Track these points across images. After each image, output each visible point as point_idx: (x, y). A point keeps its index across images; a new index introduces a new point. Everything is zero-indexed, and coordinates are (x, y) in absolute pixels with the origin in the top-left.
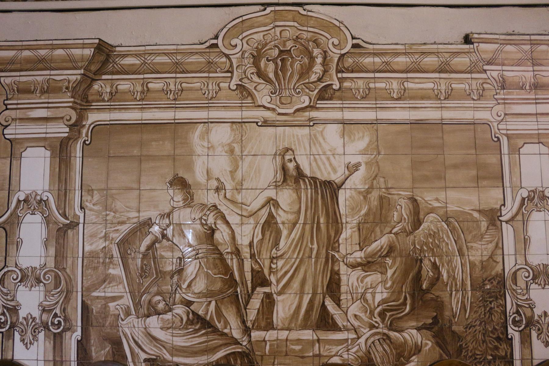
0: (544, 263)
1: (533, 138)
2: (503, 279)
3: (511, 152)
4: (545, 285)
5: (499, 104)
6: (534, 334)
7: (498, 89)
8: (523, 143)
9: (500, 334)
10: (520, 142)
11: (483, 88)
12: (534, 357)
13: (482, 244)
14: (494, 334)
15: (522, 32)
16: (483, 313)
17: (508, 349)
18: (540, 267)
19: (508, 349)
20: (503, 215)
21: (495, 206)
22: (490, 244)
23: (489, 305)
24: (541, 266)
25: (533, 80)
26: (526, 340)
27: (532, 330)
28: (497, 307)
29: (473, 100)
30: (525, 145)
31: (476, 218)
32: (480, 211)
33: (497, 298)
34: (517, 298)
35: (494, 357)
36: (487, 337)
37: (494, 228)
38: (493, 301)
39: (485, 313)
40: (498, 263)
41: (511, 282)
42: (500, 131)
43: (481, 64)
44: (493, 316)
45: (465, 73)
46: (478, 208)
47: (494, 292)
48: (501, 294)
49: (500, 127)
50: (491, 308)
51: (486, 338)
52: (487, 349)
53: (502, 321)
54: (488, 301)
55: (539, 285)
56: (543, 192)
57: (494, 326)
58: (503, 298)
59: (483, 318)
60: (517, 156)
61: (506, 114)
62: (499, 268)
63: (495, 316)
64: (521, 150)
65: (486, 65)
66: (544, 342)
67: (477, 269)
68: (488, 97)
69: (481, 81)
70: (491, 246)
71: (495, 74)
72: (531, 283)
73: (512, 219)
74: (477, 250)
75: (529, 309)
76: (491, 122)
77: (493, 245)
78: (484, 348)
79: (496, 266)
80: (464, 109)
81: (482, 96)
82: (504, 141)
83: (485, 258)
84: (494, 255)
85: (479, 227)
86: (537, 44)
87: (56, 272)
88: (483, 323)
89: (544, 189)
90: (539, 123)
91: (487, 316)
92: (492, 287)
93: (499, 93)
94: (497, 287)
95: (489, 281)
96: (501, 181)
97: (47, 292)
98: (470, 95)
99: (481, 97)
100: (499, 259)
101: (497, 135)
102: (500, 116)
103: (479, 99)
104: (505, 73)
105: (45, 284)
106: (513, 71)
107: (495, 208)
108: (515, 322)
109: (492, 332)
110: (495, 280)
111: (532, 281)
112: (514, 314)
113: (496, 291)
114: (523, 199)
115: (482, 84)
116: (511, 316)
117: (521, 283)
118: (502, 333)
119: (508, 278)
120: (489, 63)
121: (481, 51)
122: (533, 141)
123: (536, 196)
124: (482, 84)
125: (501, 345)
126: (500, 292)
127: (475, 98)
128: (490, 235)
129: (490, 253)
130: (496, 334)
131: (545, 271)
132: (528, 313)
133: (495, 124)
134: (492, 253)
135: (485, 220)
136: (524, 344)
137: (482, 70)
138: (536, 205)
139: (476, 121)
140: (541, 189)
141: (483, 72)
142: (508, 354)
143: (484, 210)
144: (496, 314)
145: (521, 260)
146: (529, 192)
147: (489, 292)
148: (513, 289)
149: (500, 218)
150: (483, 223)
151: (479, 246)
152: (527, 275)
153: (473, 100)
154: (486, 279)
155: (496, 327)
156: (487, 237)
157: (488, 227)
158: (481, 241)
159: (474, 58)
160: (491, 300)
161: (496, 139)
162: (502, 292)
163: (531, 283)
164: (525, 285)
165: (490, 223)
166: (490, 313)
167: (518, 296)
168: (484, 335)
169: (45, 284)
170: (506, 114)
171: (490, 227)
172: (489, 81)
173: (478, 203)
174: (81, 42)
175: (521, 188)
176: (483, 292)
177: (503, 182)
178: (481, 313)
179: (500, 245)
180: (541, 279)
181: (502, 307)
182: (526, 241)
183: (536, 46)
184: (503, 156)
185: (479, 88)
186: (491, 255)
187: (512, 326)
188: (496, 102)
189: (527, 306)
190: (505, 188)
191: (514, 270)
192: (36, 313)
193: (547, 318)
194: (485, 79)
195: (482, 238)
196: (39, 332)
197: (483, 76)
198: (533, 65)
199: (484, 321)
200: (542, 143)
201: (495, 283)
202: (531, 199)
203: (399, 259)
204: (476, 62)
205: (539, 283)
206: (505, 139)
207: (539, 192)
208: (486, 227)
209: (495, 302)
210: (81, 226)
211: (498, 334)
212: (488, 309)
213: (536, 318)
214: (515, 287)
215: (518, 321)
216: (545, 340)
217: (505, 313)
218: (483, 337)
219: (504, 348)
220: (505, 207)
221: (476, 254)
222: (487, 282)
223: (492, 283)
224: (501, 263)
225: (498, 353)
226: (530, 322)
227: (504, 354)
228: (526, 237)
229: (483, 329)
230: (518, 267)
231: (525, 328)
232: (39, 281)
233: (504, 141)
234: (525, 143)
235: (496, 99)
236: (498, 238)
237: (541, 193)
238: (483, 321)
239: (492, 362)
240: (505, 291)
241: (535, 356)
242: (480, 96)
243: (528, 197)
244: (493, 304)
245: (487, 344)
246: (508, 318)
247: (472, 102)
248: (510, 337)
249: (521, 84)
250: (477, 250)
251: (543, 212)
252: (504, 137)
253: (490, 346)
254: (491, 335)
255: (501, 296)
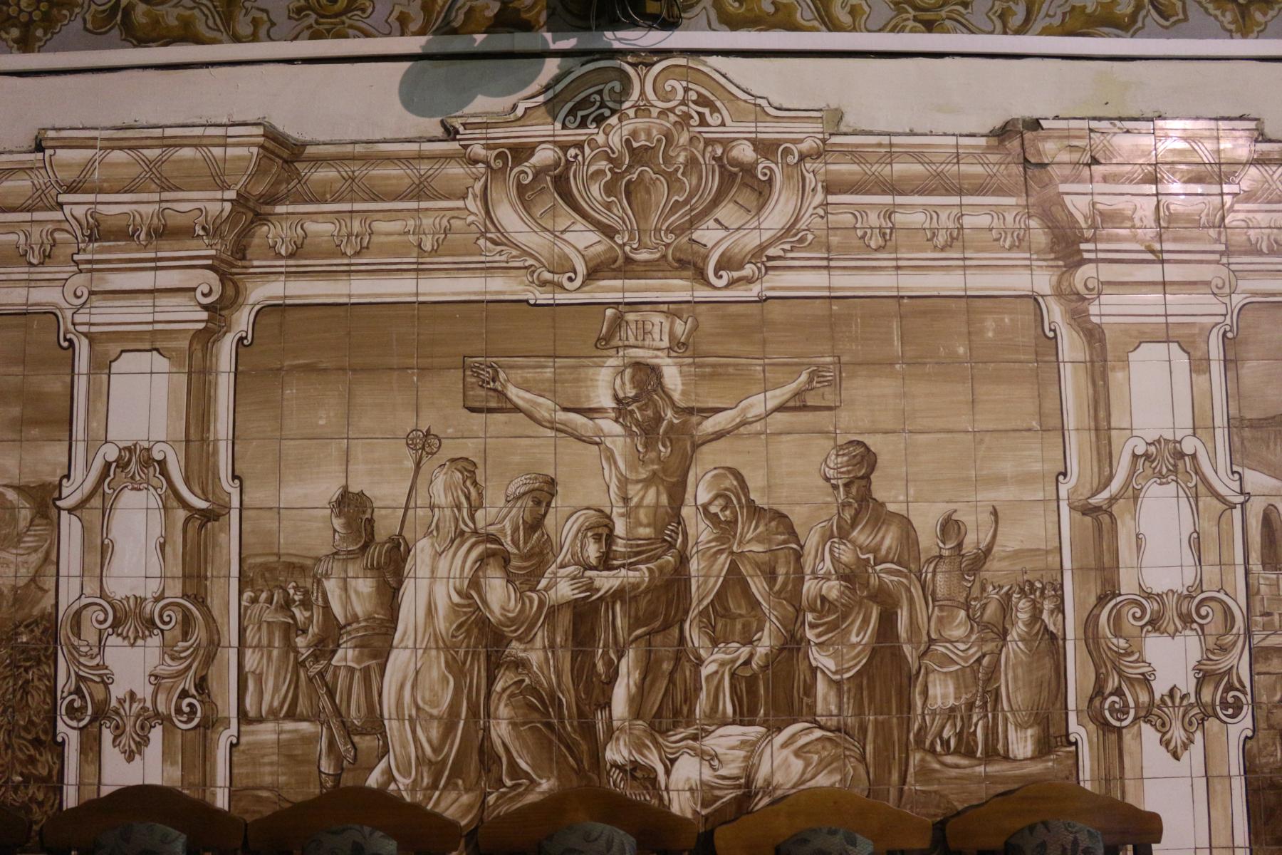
0: (138, 595)
1: (142, 340)
2: (54, 622)
3: (94, 369)
4: (135, 640)
5: (81, 271)
6: (107, 736)
7: (83, 241)
8: (119, 349)
9: (40, 733)
10: (114, 349)
11: (54, 240)
12: (104, 780)
13: (17, 554)
14: (29, 733)
15: (153, 121)
16: (11, 689)
17: (54, 763)
18: (128, 602)
19: (54, 763)
20: (63, 496)
21: (49, 479)
22: (34, 555)
23: (24, 674)
24: (132, 601)
25: (155, 221)
26: (90, 747)
27: (103, 727)
28: (39, 679)
29: (31, 265)
30: (124, 354)
31: (11, 501)
32: (19, 489)
33: (39, 662)
34: (80, 663)
35: (27, 779)
36: (16, 737)
37: (45, 522)
38: (30, 667)
39: (14, 690)
40: (46, 591)
41: (69, 630)
42: (77, 327)
43: (54, 192)
44: (29, 697)
45: (21, 211)
46: (16, 482)
47: (34, 649)
48: (49, 653)
49: (78, 319)
50: (27, 682)
51: (14, 740)
52: (13, 764)
53: (46, 707)
54: (21, 666)
55: (124, 638)
56: (149, 450)
57: (30, 717)
58: (51, 663)
59: (9, 700)
60: (105, 377)
61: (92, 293)
62: (48, 602)
63: (33, 696)
64: (114, 364)
65: (65, 193)
66: (125, 752)
67: (5, 604)
68: (62, 258)
69: (50, 227)
70: (35, 558)
71: (80, 211)
72: (109, 635)
73: (82, 504)
74: (8, 566)
75: (102, 685)
76: (61, 309)
77: (40, 555)
78: (7, 760)
79: (43, 597)
80: (11, 284)
81: (49, 256)
82: (83, 347)
83: (21, 582)
84: (40, 576)
85: (15, 520)
86: (175, 146)
87: (185, 606)
88: (10, 710)
89: (152, 444)
90: (157, 309)
91: (18, 697)
92: (32, 639)
93: (84, 250)
94: (41, 640)
95: (27, 626)
96: (68, 428)
97: (168, 650)
98: (25, 255)
99: (47, 260)
100: (49, 584)
101: (69, 336)
102: (79, 297)
103: (42, 264)
104: (99, 207)
105: (162, 631)
106: (148, 202)
107: (50, 483)
108: (72, 712)
109: (26, 729)
110: (37, 625)
111: (110, 630)
112: (70, 694)
113: (38, 647)
114: (108, 465)
115: (52, 234)
116: (64, 698)
117: (89, 634)
118: (45, 732)
119: (64, 624)
120: (71, 189)
121: (57, 166)
122: (139, 346)
123: (134, 460)
124: (52, 234)
125: (41, 755)
126: (46, 649)
127: (35, 261)
128: (35, 535)
129: (32, 571)
130: (34, 732)
131: (138, 611)
132: (100, 694)
133: (69, 314)
134: (36, 572)
135: (28, 506)
136: (86, 755)
137: (54, 204)
138: (133, 477)
139: (32, 309)
140: (146, 445)
141: (58, 208)
142: (55, 772)
143: (29, 487)
144: (34, 693)
145: (91, 588)
146: (120, 450)
147: (24, 650)
148: (72, 644)
149: (58, 503)
150: (23, 511)
151: (12, 558)
152: (101, 617)
153: (31, 265)
154: (21, 623)
155: (34, 718)
156: (29, 541)
157: (32, 521)
158: (16, 548)
159: (41, 179)
160: (28, 664)
161: (65, 344)
162: (51, 650)
163: (109, 635)
164: (96, 638)
165: (38, 513)
166: (24, 691)
167: (82, 660)
168: (9, 733)
169: (162, 631)
170: (92, 293)
171: (37, 521)
172: (66, 226)
173: (17, 471)
174: (157, 133)
175: (106, 442)
176: (12, 649)
177: (71, 431)
178: (7, 689)
179: (54, 557)
180: (129, 628)
181: (49, 681)
182: (105, 550)
183: (172, 150)
184: (76, 377)
185: (45, 241)
186: (35, 576)
187: (65, 718)
188: (75, 269)
189: (97, 679)
190: (74, 443)
191: (76, 606)
192: (145, 691)
193: (135, 705)
194: (59, 221)
195: (19, 541)
196: (151, 727)
197: (58, 215)
198: (163, 189)
199: (13, 707)
200: (157, 350)
201: (38, 632)
202: (122, 464)
203: (1023, 604)
204: (44, 187)
205: (125, 634)
206: (85, 342)
207: (141, 451)
208: (29, 520)
209: (35, 670)
210: (235, 515)
211: (37, 733)
212: (20, 683)
213: (114, 703)
214: (76, 641)
215: (77, 710)
216: (127, 748)
217: (53, 690)
218: (6, 738)
219: (47, 761)
220: (69, 480)
221: (5, 573)
222: (22, 629)
223: (32, 631)
224: (52, 593)
225: (34, 771)
226: (102, 712)
227: (45, 772)
228: (106, 541)
229: (9, 723)
230: (84, 601)
231: (90, 722)
232: (150, 624)
233: (83, 347)
234: (123, 351)
235: (77, 263)
236: (51, 544)
237: (146, 454)
238: (10, 707)
239: (22, 788)
240: (56, 649)
241: (105, 780)
242: (45, 256)
243: (120, 458)
244: (31, 673)
245: (13, 752)
246: (59, 702)
247: (26, 270)
248: (59, 739)
249: (130, 229)
250: (8, 566)
251: (145, 491)
252: (83, 338)
253: (21, 756)
254: (23, 734)
255: (47, 657)
